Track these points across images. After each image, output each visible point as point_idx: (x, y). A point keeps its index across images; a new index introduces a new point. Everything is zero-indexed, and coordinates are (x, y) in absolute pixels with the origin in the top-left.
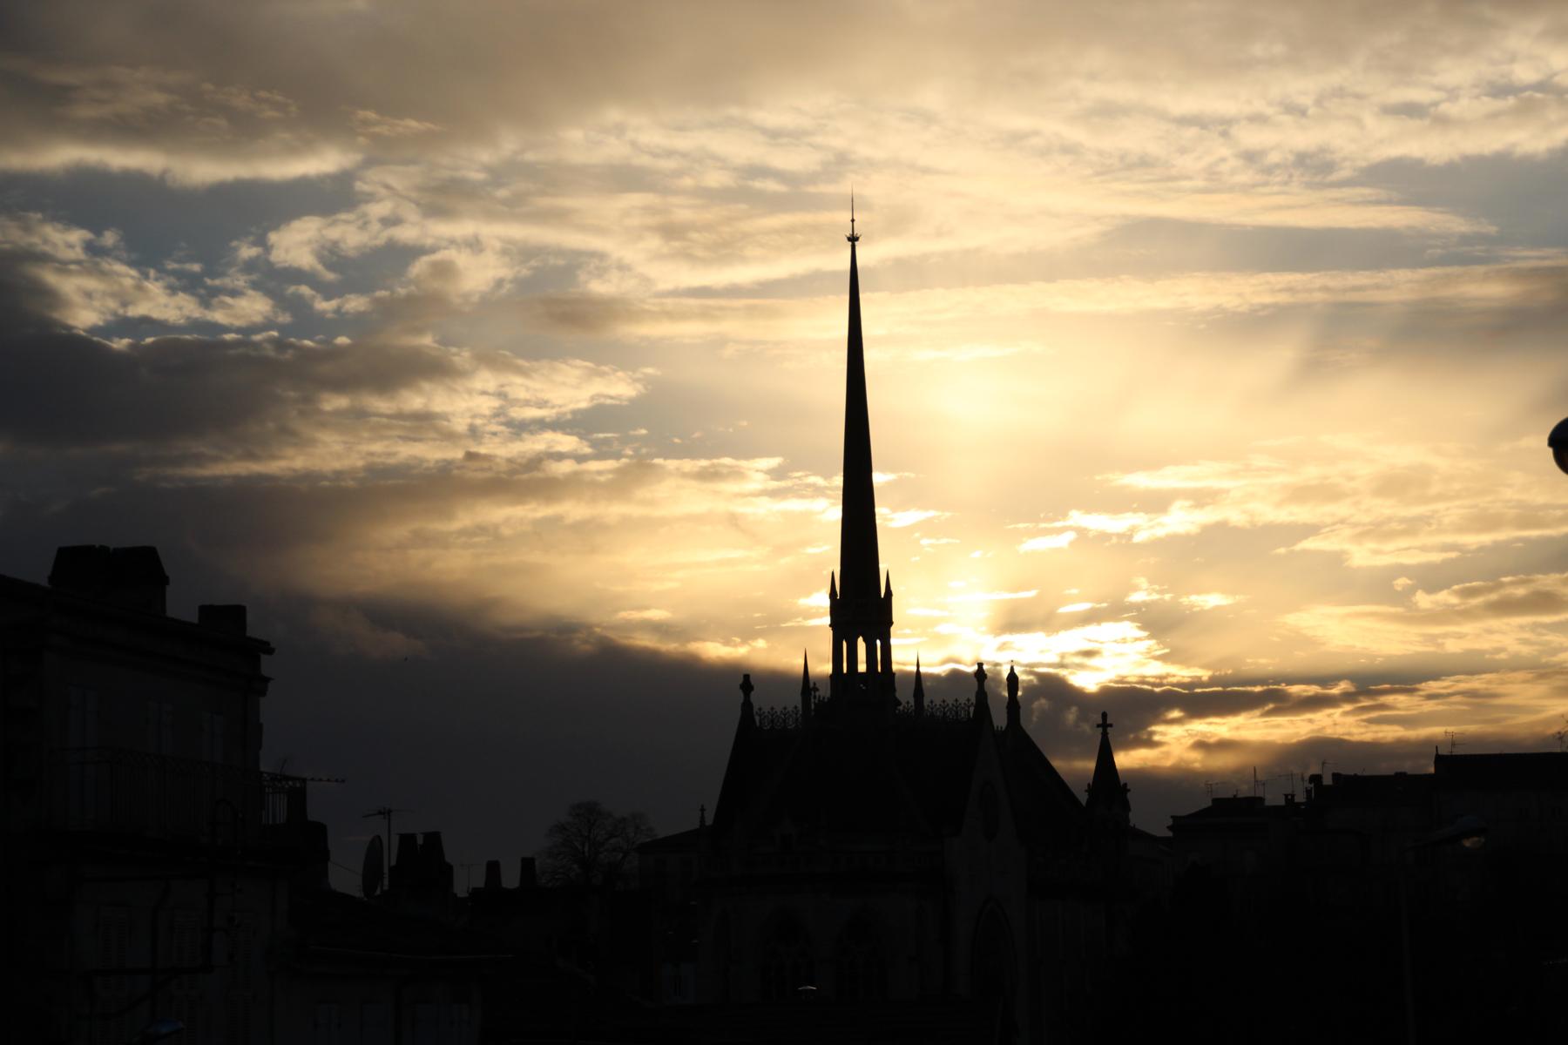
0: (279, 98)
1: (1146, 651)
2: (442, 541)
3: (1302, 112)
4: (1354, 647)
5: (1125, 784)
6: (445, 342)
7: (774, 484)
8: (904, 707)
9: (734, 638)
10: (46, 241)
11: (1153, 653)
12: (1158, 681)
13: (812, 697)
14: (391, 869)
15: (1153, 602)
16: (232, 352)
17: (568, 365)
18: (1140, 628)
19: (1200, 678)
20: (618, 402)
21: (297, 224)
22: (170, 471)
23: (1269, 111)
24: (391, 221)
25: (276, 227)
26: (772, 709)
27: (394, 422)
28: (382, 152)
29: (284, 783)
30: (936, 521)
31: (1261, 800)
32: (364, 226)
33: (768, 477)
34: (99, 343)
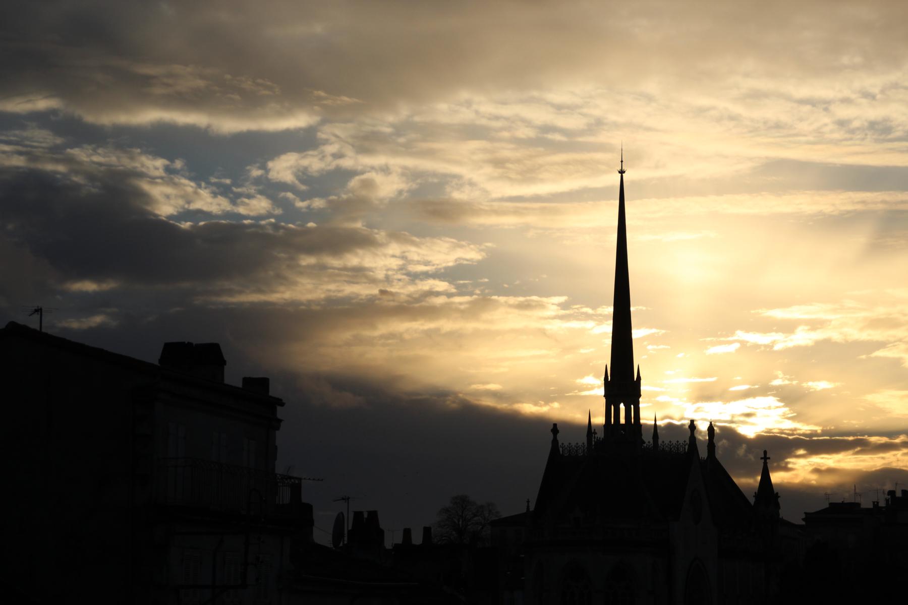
0: (269, 83)
2: (370, 342)
3: (873, 97)
5: (777, 493)
6: (370, 226)
7: (563, 312)
8: (647, 444)
9: (540, 402)
10: (143, 165)
11: (786, 416)
12: (791, 432)
14: (349, 531)
15: (786, 386)
16: (249, 230)
19: (816, 431)
20: (471, 263)
21: (284, 157)
22: (214, 299)
23: (853, 96)
24: (338, 156)
25: (272, 158)
26: (570, 444)
27: (342, 272)
28: (331, 115)
30: (656, 335)
31: (859, 504)
32: (322, 158)
33: (559, 308)
34: (174, 224)
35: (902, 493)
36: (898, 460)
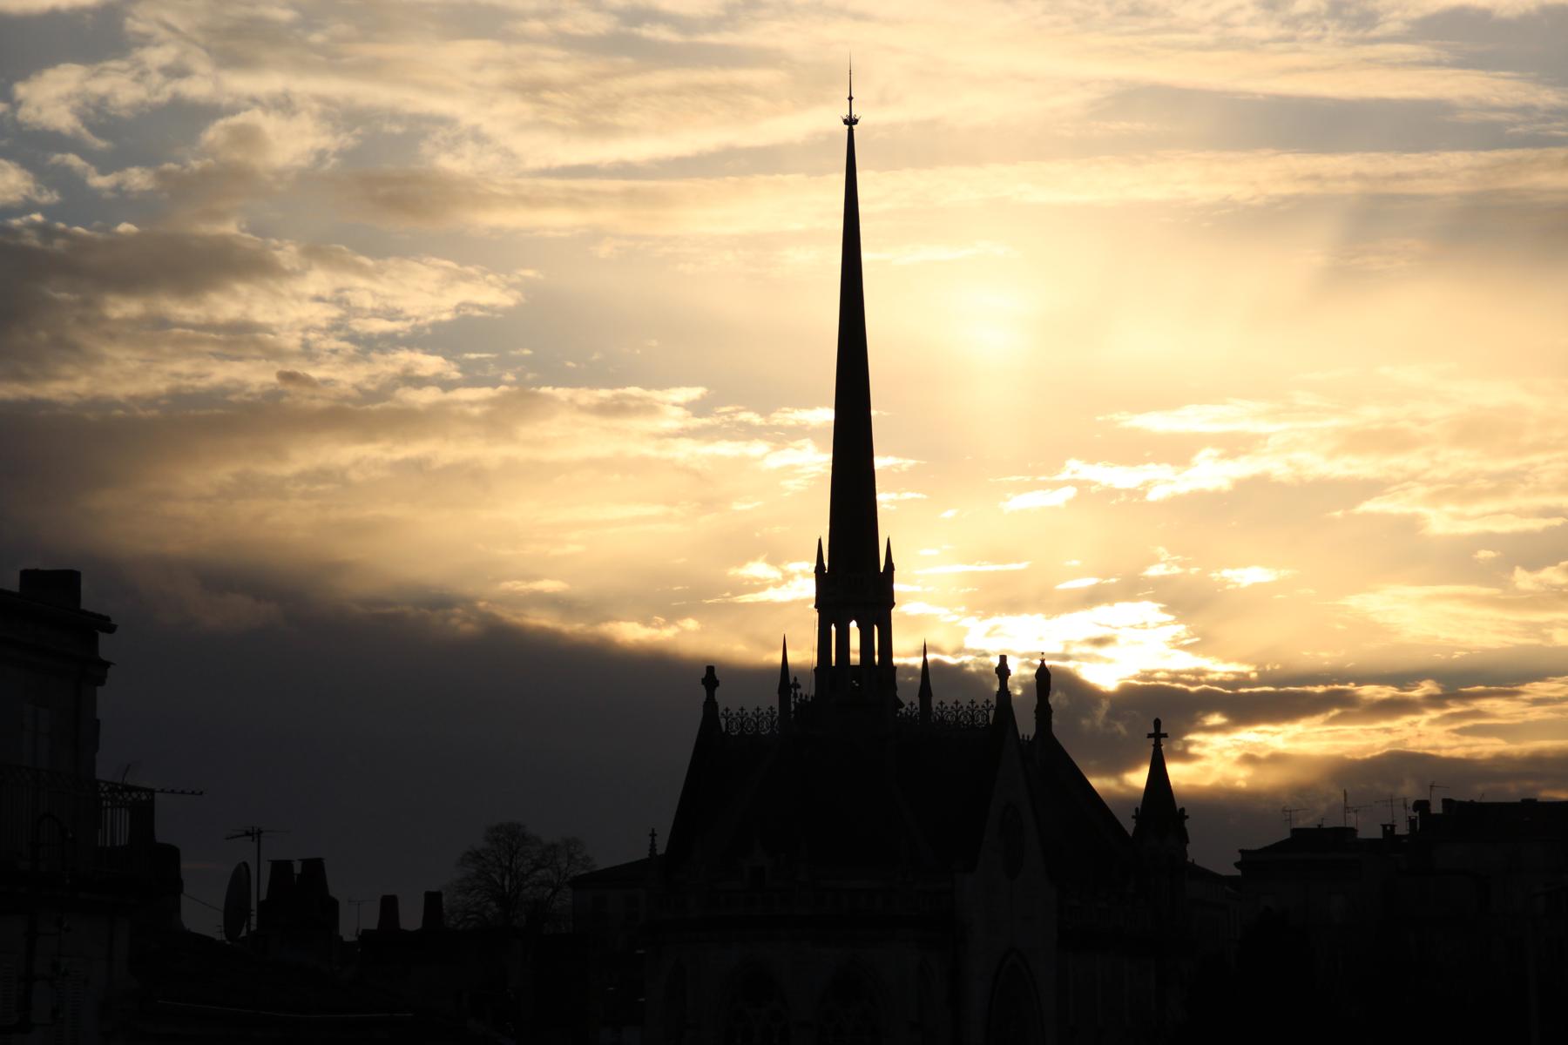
1: (1171, 639)
2: (277, 489)
4: (1437, 637)
5: (1183, 810)
9: (656, 617)
12: (1193, 678)
13: (792, 695)
14: (261, 905)
15: (1173, 578)
17: (425, 264)
18: (1163, 610)
19: (1246, 675)
24: (177, 71)
25: (24, 77)
27: (204, 335)
29: (126, 794)
30: (895, 470)
31: (1352, 831)
32: (141, 76)
33: (689, 413)
35: (1443, 807)
36: (1419, 735)
